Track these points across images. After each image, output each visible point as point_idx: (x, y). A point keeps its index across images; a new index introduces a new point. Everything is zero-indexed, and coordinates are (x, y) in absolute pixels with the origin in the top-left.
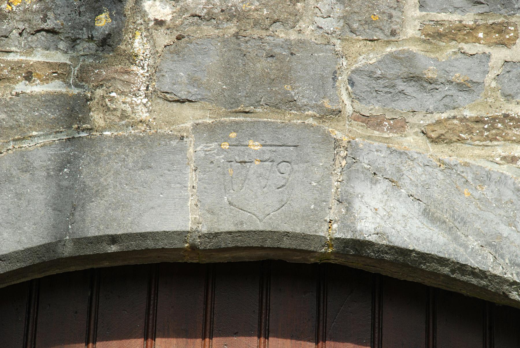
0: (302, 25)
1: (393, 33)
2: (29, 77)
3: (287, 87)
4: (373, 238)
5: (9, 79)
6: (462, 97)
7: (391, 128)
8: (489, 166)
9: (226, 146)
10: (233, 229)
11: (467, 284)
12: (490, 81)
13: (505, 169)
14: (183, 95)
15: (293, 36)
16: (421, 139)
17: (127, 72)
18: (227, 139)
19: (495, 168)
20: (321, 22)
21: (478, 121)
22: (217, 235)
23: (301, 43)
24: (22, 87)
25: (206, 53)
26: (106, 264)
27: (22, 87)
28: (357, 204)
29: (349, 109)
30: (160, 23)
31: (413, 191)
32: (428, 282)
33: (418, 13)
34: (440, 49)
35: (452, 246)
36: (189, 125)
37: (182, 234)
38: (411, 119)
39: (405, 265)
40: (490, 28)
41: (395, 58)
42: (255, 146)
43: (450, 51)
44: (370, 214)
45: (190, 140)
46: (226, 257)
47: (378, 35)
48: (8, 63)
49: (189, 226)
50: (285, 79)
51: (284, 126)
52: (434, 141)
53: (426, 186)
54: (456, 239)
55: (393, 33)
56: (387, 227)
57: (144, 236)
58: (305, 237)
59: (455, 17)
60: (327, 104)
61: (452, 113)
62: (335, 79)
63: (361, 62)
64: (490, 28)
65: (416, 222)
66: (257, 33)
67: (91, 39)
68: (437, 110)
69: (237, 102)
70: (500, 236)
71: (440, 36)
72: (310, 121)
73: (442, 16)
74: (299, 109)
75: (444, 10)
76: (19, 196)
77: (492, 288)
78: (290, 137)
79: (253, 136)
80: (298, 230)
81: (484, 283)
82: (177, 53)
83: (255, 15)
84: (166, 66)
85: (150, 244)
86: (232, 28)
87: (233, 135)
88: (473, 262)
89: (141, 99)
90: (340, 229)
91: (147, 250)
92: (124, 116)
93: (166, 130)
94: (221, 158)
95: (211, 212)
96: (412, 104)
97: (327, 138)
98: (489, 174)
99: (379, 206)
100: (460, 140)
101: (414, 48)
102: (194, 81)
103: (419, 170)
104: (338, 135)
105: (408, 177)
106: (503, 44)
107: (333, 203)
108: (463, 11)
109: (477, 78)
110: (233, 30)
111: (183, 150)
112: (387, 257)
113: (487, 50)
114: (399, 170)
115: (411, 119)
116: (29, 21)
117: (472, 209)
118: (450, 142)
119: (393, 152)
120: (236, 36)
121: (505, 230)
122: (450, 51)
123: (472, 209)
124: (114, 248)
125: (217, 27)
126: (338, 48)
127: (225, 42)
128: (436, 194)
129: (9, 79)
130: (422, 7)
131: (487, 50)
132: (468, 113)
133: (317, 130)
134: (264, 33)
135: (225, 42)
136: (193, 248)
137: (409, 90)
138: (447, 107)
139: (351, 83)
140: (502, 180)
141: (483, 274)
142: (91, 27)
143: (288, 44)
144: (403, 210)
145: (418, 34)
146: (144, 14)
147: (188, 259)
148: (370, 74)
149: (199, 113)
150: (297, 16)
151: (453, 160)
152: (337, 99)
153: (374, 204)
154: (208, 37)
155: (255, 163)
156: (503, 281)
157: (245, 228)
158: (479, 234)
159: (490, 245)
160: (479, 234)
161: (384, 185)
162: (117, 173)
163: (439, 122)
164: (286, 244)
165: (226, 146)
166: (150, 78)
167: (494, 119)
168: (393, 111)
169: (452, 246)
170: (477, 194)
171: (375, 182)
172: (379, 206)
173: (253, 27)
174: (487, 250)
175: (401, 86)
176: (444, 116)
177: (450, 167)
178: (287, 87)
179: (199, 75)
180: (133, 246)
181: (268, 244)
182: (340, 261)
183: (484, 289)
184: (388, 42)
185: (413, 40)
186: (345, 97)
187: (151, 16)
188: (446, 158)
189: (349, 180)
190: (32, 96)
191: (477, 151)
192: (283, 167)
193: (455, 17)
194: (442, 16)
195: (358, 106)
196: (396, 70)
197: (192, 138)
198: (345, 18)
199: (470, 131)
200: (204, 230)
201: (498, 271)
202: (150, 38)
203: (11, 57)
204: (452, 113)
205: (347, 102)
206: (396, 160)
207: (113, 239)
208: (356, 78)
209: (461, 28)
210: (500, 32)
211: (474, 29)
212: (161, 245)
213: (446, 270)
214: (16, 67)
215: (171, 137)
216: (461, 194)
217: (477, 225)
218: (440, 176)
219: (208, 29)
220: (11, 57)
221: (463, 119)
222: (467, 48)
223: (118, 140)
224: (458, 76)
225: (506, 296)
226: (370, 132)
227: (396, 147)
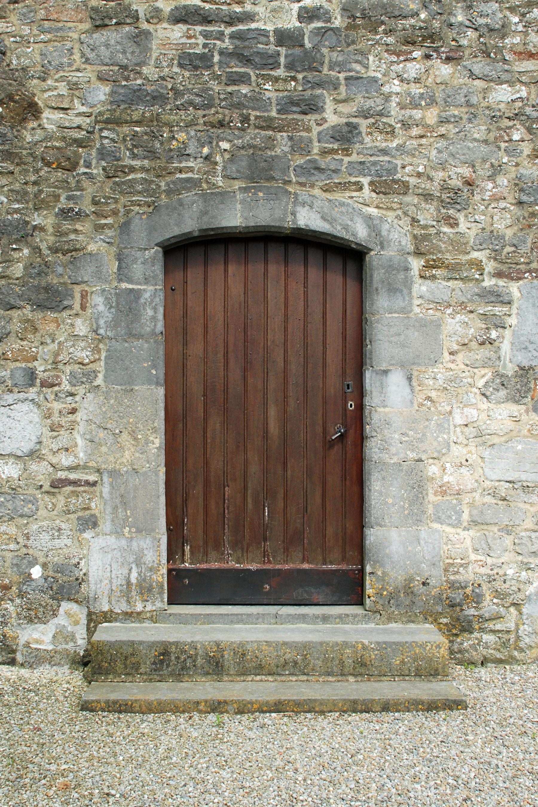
0: (276, 149)
1: (309, 152)
2: (180, 172)
3: (272, 172)
4: (304, 227)
5: (174, 173)
6: (334, 175)
7: (309, 187)
8: (344, 200)
9: (250, 195)
10: (254, 225)
11: (336, 242)
12: (343, 169)
13: (349, 201)
14: (234, 176)
15: (273, 154)
16: (320, 190)
17: (215, 169)
18: (251, 192)
19: (345, 200)
20: (283, 148)
21: (340, 183)
22: (248, 227)
23: (276, 156)
24: (178, 175)
25: (242, 161)
26: (210, 238)
27: (178, 175)
28: (298, 215)
29: (294, 180)
30: (225, 150)
31: (318, 209)
32: (323, 242)
33: (317, 144)
34: (326, 157)
35: (331, 229)
36: (237, 187)
37: (236, 227)
38: (317, 183)
39: (315, 236)
40: (343, 150)
41: (310, 161)
42: (261, 194)
43: (329, 158)
44: (303, 218)
45: (238, 193)
46: (252, 235)
47: (304, 152)
48: (173, 167)
49: (238, 224)
50: (271, 169)
51: (271, 187)
52: (325, 191)
53: (322, 208)
54: (333, 226)
55: (309, 152)
56: (309, 223)
57: (223, 228)
58: (279, 227)
59: (331, 146)
60: (286, 178)
61: (331, 181)
62: (289, 169)
63: (298, 163)
64: (343, 150)
65: (319, 221)
66: (260, 153)
67: (201, 157)
68: (325, 180)
69: (254, 179)
70: (348, 225)
71: (325, 152)
72: (280, 185)
73: (326, 145)
74: (276, 180)
75: (327, 143)
76: (179, 214)
77: (345, 243)
78: (273, 191)
79: (260, 191)
80: (277, 225)
81: (342, 242)
82: (232, 161)
83: (259, 146)
84: (228, 166)
85: (225, 231)
86: (251, 151)
87: (253, 191)
88: (339, 235)
89: (220, 178)
90: (292, 224)
91: (224, 233)
92: (214, 185)
93: (229, 190)
94: (249, 199)
95: (246, 219)
96: (317, 178)
97: (286, 191)
98: (344, 203)
99: (306, 215)
100: (334, 191)
101: (317, 157)
102: (238, 171)
103: (320, 202)
104: (290, 190)
105: (316, 204)
106: (348, 155)
107: (289, 215)
108: (334, 143)
109: (339, 168)
110: (252, 152)
111: (235, 197)
112: (310, 234)
113: (342, 158)
114: (312, 202)
115: (317, 183)
116: (180, 152)
117: (338, 215)
118: (330, 192)
119: (310, 195)
120: (253, 154)
121: (349, 223)
122: (329, 158)
123: (338, 215)
124: (212, 233)
125: (246, 151)
126: (290, 158)
127: (249, 156)
128: (325, 210)
129: (174, 173)
130: (319, 142)
131: (342, 158)
132: (336, 181)
133: (282, 188)
134: (263, 153)
135: (249, 156)
136: (240, 232)
137: (315, 173)
138: (329, 179)
139: (295, 170)
140: (348, 205)
141: (342, 239)
142: (201, 153)
143: (272, 157)
144: (314, 217)
145: (318, 152)
146: (220, 147)
147: (238, 236)
148: (302, 167)
149: (240, 183)
150: (274, 146)
151: (331, 198)
152: (289, 176)
153: (304, 215)
154: (243, 155)
155: (483, 190)
156: (348, 241)
157: (258, 224)
158: (341, 224)
159: (344, 228)
160: (341, 224)
161: (307, 208)
162: (212, 206)
163: (326, 184)
164: (273, 230)
165: (250, 195)
166: (223, 171)
167: (345, 183)
168: (310, 181)
169: (331, 229)
170: (340, 210)
171: (304, 207)
172: (306, 215)
173: (509, 778)
174: (343, 230)
175: (312, 171)
176: (328, 182)
177: (330, 201)
178: (272, 172)
179: (240, 169)
180: (219, 232)
181: (267, 230)
182: (292, 235)
183: (342, 244)
184: (307, 155)
185: (316, 154)
186: (292, 175)
187: (222, 148)
188: (329, 197)
189: (295, 206)
190: (182, 178)
191: (340, 195)
192: (271, 202)
193: (331, 146)
194: (326, 145)
195: (297, 179)
196: (310, 166)
197: (238, 192)
198: (292, 147)
199: (337, 187)
200: (244, 225)
201: (347, 238)
202: (222, 156)
203: (174, 165)
204: (331, 181)
205: (294, 177)
206: (311, 198)
207: (212, 229)
208: (296, 168)
209: (333, 149)
210: (347, 151)
211: (338, 150)
212: (229, 231)
213: (329, 238)
214: (176, 168)
215: (231, 192)
216: (334, 210)
217: (340, 221)
218: (327, 204)
219: (243, 152)
220: (174, 165)
221: (335, 183)
222: (335, 157)
223: (212, 193)
224: (332, 167)
225: (350, 246)
226: (302, 188)
227: (311, 193)
